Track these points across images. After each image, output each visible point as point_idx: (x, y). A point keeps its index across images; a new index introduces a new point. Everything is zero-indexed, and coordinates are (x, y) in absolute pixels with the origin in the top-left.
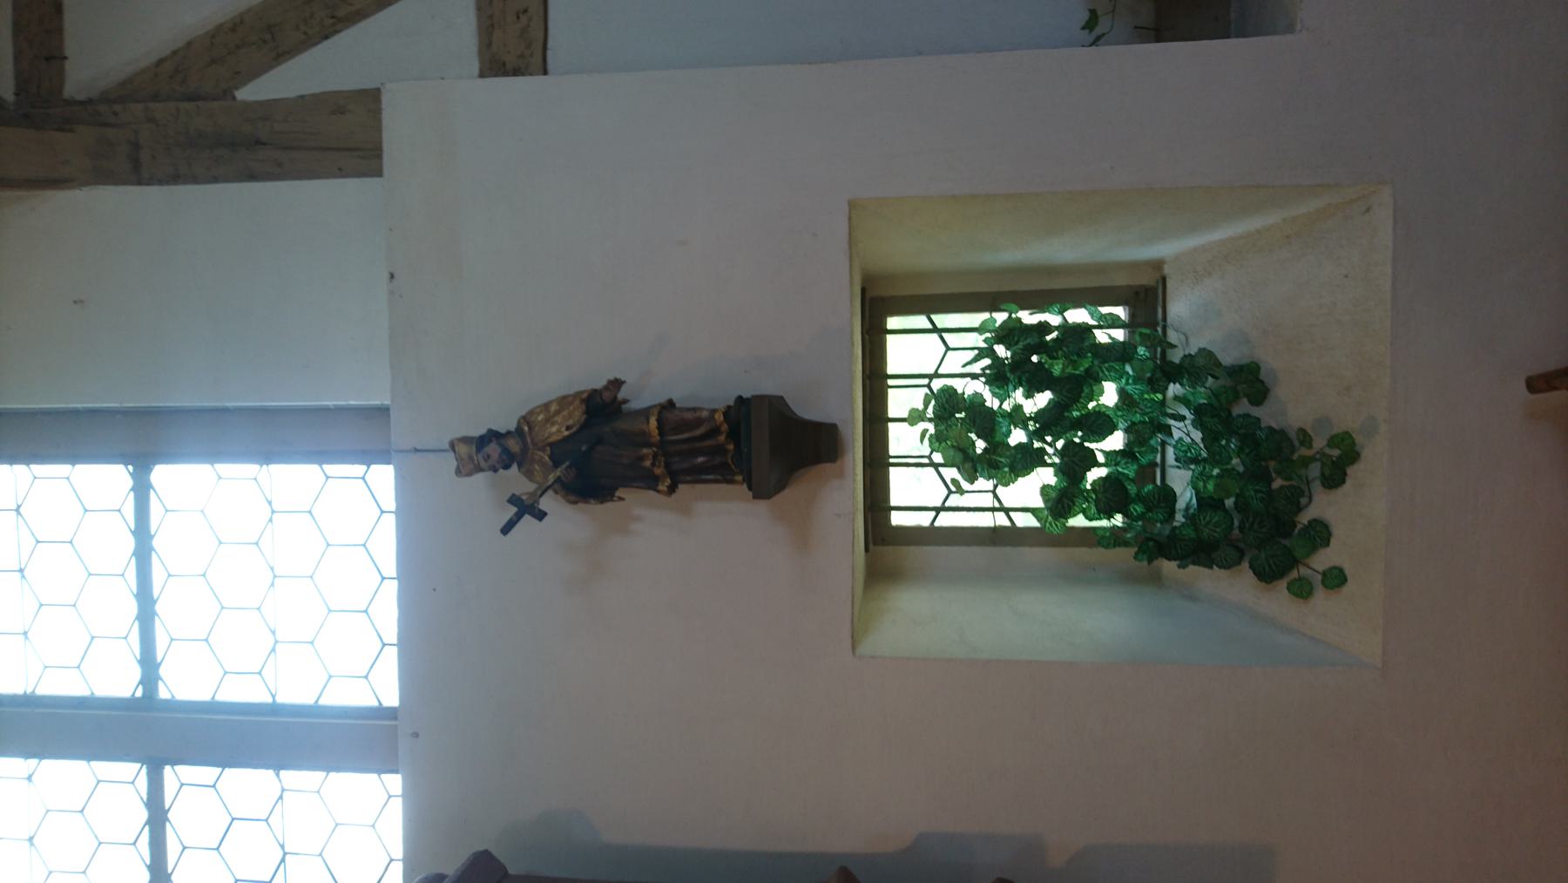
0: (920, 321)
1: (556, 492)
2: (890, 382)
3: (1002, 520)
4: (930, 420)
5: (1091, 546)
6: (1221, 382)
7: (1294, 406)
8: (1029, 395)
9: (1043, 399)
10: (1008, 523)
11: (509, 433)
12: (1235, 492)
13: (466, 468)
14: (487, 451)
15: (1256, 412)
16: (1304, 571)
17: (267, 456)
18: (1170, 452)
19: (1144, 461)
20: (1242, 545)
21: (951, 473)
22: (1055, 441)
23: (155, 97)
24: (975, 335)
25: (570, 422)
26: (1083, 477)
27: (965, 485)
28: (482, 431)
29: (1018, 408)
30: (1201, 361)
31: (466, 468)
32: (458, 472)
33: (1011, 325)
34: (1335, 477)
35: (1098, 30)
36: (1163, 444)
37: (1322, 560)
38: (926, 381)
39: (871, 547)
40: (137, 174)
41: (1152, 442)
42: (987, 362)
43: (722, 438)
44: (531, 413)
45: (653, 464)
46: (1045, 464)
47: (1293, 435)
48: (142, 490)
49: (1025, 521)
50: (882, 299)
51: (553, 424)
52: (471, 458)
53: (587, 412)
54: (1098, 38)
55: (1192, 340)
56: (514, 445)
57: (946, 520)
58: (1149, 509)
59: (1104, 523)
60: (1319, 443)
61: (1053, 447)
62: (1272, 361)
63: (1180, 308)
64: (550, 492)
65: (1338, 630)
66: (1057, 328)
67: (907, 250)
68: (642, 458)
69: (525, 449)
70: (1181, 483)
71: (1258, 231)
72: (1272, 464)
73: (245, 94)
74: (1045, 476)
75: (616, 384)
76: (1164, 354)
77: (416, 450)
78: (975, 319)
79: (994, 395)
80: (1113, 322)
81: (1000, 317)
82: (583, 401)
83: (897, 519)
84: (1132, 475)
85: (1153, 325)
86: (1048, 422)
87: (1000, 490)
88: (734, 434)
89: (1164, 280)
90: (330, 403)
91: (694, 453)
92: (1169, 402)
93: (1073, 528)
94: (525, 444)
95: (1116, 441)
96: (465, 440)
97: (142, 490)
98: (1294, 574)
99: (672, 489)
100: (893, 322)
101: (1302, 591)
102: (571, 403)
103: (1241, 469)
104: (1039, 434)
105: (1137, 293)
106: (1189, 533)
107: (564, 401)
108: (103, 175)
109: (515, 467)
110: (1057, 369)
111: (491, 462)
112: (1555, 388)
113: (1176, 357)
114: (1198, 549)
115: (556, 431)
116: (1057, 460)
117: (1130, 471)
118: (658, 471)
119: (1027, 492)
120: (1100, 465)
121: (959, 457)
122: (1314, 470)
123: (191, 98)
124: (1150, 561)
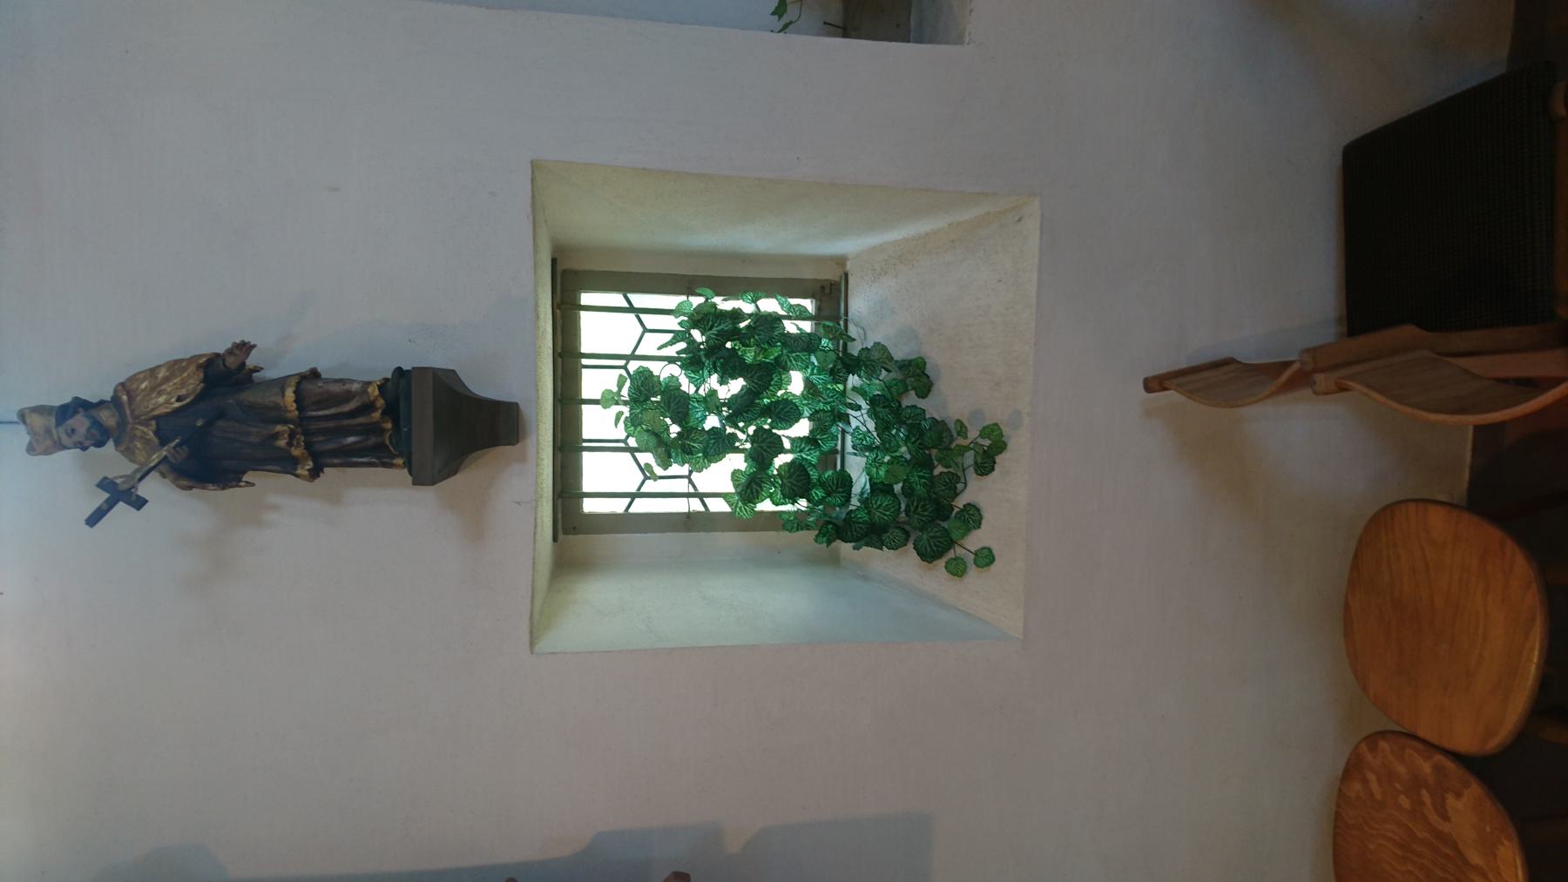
0: (616, 299)
1: (163, 475)
2: (585, 362)
3: (696, 505)
4: (625, 403)
5: (777, 530)
6: (893, 375)
7: (950, 402)
8: (722, 382)
9: (737, 385)
10: (702, 509)
11: (102, 403)
12: (904, 485)
14: (75, 423)
15: (922, 403)
16: (959, 551)
18: (849, 438)
19: (825, 448)
20: (907, 527)
21: (646, 458)
22: (746, 427)
24: (671, 317)
25: (183, 392)
26: (771, 463)
27: (659, 471)
28: (67, 400)
29: (713, 393)
30: (876, 355)
31: (43, 445)
32: (31, 449)
33: (706, 309)
34: (986, 466)
35: (785, 19)
36: (844, 432)
37: (975, 541)
38: (622, 363)
39: (561, 536)
41: (833, 429)
42: (682, 345)
43: (377, 415)
44: (132, 379)
45: (290, 444)
46: (737, 450)
47: (952, 426)
49: (718, 506)
50: (576, 273)
51: (160, 394)
52: (48, 431)
53: (205, 380)
54: (785, 27)
55: (869, 334)
56: (108, 418)
57: (641, 506)
58: (829, 495)
59: (789, 507)
60: (973, 434)
61: (743, 435)
62: (937, 358)
63: (860, 303)
64: (154, 475)
65: (988, 601)
66: (750, 315)
67: (601, 223)
68: (276, 436)
69: (122, 424)
70: (857, 469)
71: (927, 234)
72: (934, 452)
74: (736, 462)
75: (245, 348)
76: (845, 346)
78: (670, 301)
79: (691, 380)
80: (801, 314)
81: (696, 301)
82: (200, 366)
83: (589, 506)
84: (814, 461)
85: (836, 319)
86: (741, 409)
87: (695, 476)
88: (391, 411)
89: (846, 275)
91: (350, 431)
92: (849, 392)
93: (762, 512)
94: (122, 416)
95: (802, 428)
96: (40, 410)
98: (951, 554)
99: (315, 473)
100: (587, 298)
101: (957, 570)
102: (185, 369)
103: (908, 457)
104: (732, 420)
105: (823, 288)
106: (863, 516)
107: (175, 366)
109: (110, 444)
110: (749, 357)
111: (76, 438)
112: (1165, 389)
113: (854, 350)
114: (869, 531)
115: (164, 402)
116: (748, 446)
117: (812, 457)
118: (296, 452)
119: (720, 476)
120: (787, 452)
121: (653, 441)
122: (969, 458)
124: (829, 543)
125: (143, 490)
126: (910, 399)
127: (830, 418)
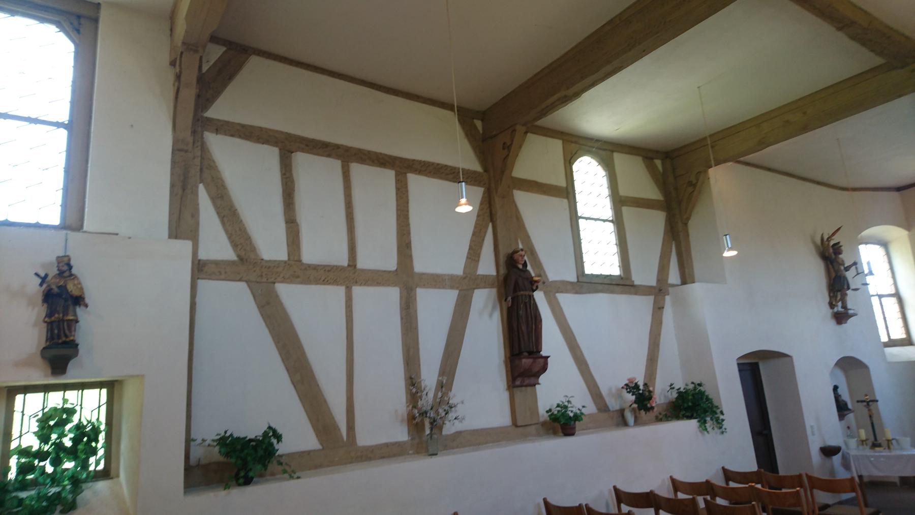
13: (59, 259)
14: (65, 268)
17: (67, 171)
21: (40, 414)
23: (202, 158)
40: (175, 150)
48: (58, 125)
56: (67, 274)
63: (102, 485)
67: (129, 394)
69: (65, 277)
73: (201, 188)
77: (66, 240)
78: (103, 419)
86: (59, 446)
88: (65, 343)
90: (87, 200)
91: (59, 330)
95: (49, 469)
96: (69, 260)
97: (58, 125)
107: (82, 289)
108: (176, 141)
110: (80, 447)
115: (71, 287)
123: (201, 170)
125: (45, 286)
126: (59, 508)
127: (54, 479)
